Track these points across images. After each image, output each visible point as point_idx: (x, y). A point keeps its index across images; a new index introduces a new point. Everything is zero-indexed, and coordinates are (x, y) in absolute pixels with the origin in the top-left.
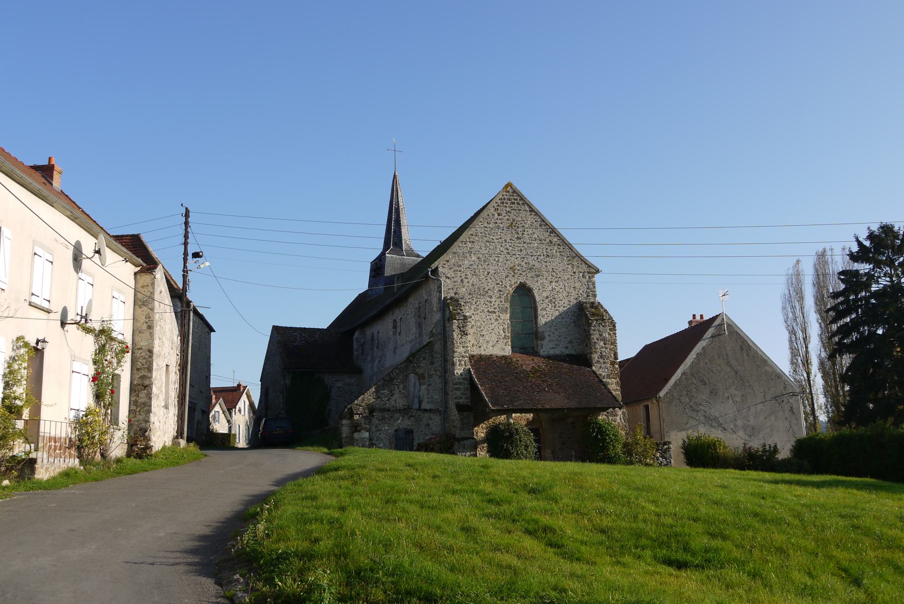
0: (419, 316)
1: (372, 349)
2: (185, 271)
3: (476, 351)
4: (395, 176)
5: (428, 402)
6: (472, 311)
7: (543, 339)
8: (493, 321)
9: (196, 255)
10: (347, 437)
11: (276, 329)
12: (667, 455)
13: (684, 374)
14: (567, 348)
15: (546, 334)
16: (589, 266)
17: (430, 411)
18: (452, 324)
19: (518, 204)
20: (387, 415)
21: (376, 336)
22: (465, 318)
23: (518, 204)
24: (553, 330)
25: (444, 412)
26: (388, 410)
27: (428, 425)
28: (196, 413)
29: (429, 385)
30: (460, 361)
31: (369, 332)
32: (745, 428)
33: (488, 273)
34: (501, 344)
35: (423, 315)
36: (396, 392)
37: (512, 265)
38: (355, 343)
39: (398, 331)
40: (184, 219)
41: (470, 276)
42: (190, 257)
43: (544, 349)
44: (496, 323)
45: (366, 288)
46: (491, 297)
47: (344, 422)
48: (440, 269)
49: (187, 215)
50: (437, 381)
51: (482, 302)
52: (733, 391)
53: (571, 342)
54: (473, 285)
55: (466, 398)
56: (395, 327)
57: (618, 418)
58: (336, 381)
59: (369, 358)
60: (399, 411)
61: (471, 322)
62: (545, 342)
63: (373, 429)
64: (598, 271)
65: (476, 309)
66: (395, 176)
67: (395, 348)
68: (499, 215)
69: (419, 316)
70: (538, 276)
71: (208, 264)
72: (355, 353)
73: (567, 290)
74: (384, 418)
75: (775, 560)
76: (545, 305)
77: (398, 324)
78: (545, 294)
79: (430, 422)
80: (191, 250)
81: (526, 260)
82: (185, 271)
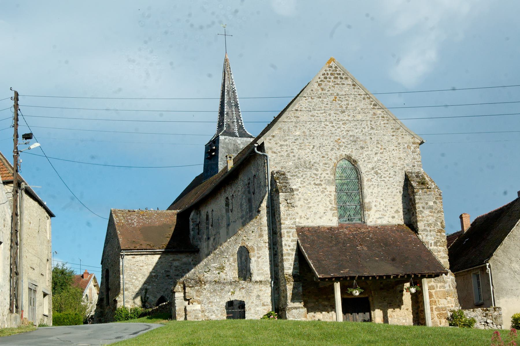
0: (249, 192)
1: (208, 228)
2: (17, 153)
3: (304, 223)
4: (226, 60)
5: (258, 275)
6: (299, 185)
7: (370, 209)
8: (320, 193)
9: (28, 137)
12: (499, 320)
15: (373, 205)
18: (278, 197)
19: (341, 78)
20: (217, 287)
22: (292, 190)
23: (341, 78)
24: (379, 200)
27: (258, 296)
28: (37, 295)
29: (258, 258)
30: (288, 232)
31: (203, 213)
34: (330, 214)
35: (252, 191)
38: (191, 223)
39: (230, 207)
40: (13, 103)
41: (296, 150)
42: (20, 138)
43: (370, 220)
44: (322, 196)
45: (202, 172)
46: (317, 170)
48: (266, 145)
49: (16, 99)
51: (309, 175)
54: (299, 159)
56: (227, 205)
57: (447, 285)
58: (174, 260)
59: (205, 237)
61: (297, 195)
65: (303, 182)
66: (226, 60)
67: (228, 225)
68: (322, 89)
69: (249, 192)
70: (362, 148)
71: (37, 145)
72: (192, 233)
73: (393, 161)
74: (215, 290)
75: (508, 261)
76: (370, 177)
77: (230, 201)
78: (370, 166)
79: (261, 294)
80: (21, 133)
82: (17, 153)
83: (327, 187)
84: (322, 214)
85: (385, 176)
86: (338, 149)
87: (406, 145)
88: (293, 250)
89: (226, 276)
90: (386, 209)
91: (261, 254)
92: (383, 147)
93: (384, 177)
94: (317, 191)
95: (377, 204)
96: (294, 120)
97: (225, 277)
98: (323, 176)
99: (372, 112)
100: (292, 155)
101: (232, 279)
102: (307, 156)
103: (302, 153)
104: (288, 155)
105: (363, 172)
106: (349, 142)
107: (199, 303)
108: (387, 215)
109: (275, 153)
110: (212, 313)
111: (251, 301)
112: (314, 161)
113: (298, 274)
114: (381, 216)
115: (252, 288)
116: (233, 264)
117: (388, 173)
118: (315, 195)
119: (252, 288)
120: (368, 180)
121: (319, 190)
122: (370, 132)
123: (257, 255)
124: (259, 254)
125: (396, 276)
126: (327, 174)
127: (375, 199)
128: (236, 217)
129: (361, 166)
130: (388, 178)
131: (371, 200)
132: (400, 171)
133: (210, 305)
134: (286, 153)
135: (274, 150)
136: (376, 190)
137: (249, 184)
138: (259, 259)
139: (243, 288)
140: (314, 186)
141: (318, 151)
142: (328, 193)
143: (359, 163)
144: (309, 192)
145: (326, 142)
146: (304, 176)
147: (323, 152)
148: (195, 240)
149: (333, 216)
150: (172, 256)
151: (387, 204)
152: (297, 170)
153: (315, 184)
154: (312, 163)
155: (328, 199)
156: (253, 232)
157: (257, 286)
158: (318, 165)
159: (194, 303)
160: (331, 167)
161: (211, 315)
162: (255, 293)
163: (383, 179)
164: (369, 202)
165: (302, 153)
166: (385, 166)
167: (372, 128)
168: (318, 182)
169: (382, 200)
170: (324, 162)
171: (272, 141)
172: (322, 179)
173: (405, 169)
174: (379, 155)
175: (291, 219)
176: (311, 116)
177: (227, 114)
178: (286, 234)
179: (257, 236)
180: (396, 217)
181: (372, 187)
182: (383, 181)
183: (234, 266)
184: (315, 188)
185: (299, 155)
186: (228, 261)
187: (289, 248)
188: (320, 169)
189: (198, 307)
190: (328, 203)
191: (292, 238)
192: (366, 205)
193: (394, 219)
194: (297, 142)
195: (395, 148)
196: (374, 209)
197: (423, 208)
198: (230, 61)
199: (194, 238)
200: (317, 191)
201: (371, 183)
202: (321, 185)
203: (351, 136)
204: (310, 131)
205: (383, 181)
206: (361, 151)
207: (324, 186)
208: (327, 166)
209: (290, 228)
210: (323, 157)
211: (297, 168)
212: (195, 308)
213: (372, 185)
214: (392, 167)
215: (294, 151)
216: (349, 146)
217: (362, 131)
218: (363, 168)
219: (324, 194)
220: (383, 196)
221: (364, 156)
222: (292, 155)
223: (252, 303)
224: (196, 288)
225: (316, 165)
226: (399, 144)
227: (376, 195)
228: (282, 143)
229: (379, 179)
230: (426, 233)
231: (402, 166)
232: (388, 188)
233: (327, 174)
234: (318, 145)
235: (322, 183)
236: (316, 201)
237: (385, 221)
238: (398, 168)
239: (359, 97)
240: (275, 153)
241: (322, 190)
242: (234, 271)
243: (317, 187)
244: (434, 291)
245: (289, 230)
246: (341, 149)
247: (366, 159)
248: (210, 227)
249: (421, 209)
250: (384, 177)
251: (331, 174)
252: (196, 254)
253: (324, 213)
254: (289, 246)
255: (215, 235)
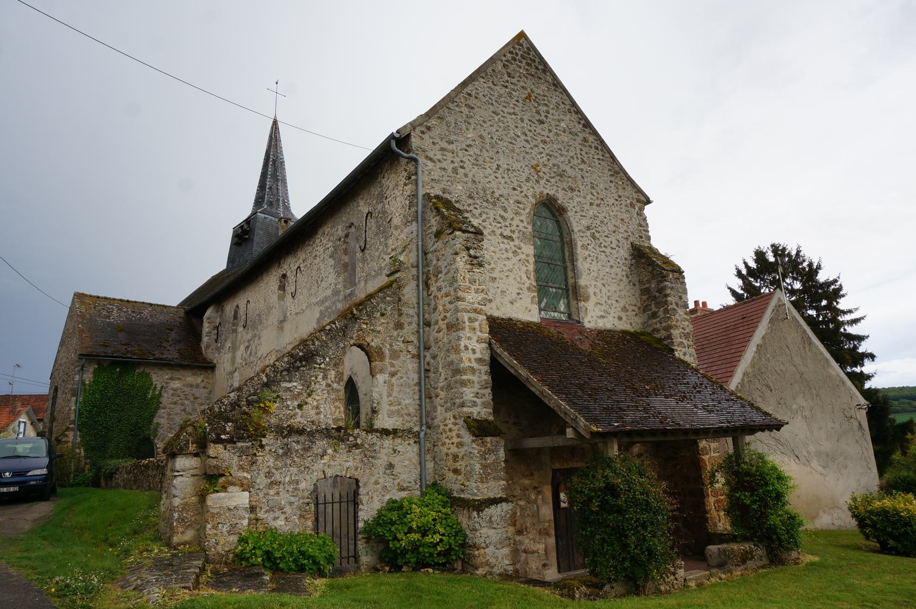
1: (235, 331)
4: (275, 123)
5: (391, 414)
7: (587, 299)
8: (510, 255)
10: (185, 507)
11: (80, 297)
13: (745, 374)
14: (620, 318)
15: (591, 291)
16: (639, 191)
17: (394, 433)
21: (242, 311)
25: (423, 433)
26: (301, 432)
27: (391, 466)
29: (393, 375)
30: (471, 320)
31: (229, 308)
32: (818, 454)
33: (498, 167)
36: (320, 386)
37: (534, 162)
41: (468, 165)
45: (224, 267)
46: (505, 210)
47: (182, 462)
50: (409, 368)
52: (801, 400)
53: (624, 309)
55: (485, 405)
58: (172, 379)
60: (326, 433)
62: (590, 305)
63: (262, 481)
64: (648, 202)
66: (275, 123)
72: (205, 339)
78: (585, 222)
79: (395, 460)
81: (553, 161)
83: (522, 245)
84: (514, 296)
85: (606, 244)
86: (537, 182)
87: (628, 202)
88: (480, 361)
89: (318, 414)
90: (609, 302)
91: (397, 368)
92: (600, 196)
93: (605, 247)
94: (507, 250)
95: (597, 291)
96: (466, 110)
97: (315, 418)
98: (515, 223)
99: (582, 135)
100: (461, 171)
101: (331, 422)
102: (487, 180)
103: (479, 174)
104: (455, 170)
105: (576, 230)
106: (553, 175)
107: (246, 486)
108: (612, 314)
109: (431, 159)
110: (278, 513)
111: (373, 480)
112: (500, 192)
113: (491, 418)
114: (602, 313)
115: (377, 448)
116: (335, 385)
117: (610, 240)
118: (503, 256)
119: (377, 448)
120: (583, 246)
121: (508, 247)
122: (581, 167)
123: (390, 369)
124: (393, 365)
125: (908, 448)
126: (522, 221)
127: (594, 283)
128: (305, 305)
129: (572, 219)
130: (609, 249)
131: (588, 283)
132: (625, 241)
133: (272, 492)
134: (451, 166)
135: (431, 154)
136: (594, 267)
137: (347, 236)
138: (394, 379)
139: (356, 446)
140: (501, 239)
141: (505, 176)
142: (524, 256)
143: (569, 214)
144: (492, 248)
145: (518, 165)
146: (484, 216)
147: (514, 180)
148: (210, 350)
149: (532, 302)
150: (169, 372)
151: (610, 294)
152: (470, 201)
153: (501, 235)
154: (496, 195)
155: (524, 269)
156: (382, 315)
157: (388, 442)
158: (506, 202)
159: (231, 488)
160: (528, 210)
161: (275, 519)
162: (383, 459)
163: (603, 249)
164: (586, 286)
165: (479, 174)
166: (605, 228)
167: (583, 162)
168: (507, 233)
169: (604, 285)
170: (516, 198)
171: (426, 136)
172: (514, 228)
173: (631, 239)
174: (595, 207)
175: (477, 291)
176: (494, 113)
177: (270, 188)
178: (467, 323)
179: (391, 325)
180: (624, 318)
181: (589, 260)
182: (603, 252)
183: (338, 391)
184: (503, 243)
185: (474, 176)
186: (325, 377)
187: (473, 357)
188: (509, 210)
189: (241, 498)
190: (524, 277)
191: (479, 333)
192: (582, 291)
193: (622, 322)
194: (471, 151)
195: (616, 202)
196: (593, 299)
197: (677, 304)
198: (280, 125)
199: (208, 347)
200: (507, 250)
201: (587, 253)
202: (510, 238)
203: (554, 165)
204: (492, 138)
205: (603, 252)
206: (570, 194)
207: (517, 242)
208: (520, 206)
209: (475, 311)
210: (514, 189)
211: (470, 197)
212: (232, 504)
213: (589, 256)
214: (614, 232)
215: (465, 165)
216: (553, 181)
217: (569, 162)
218: (577, 222)
219: (518, 258)
220: (605, 278)
221: (575, 204)
222: (461, 171)
223: (377, 483)
224: (239, 444)
225: (503, 200)
226: (620, 197)
227: (595, 274)
228: (446, 145)
229: (597, 248)
230: (683, 350)
231: (626, 234)
232: (612, 267)
233: (522, 221)
234: (505, 166)
235: (514, 236)
236: (505, 269)
237: (608, 324)
238: (621, 235)
239: (563, 106)
240: (431, 159)
241: (514, 249)
242: (337, 404)
243: (506, 241)
244: (707, 456)
245: (473, 315)
246: (542, 182)
247: (578, 209)
248: (241, 329)
249: (674, 306)
250: (605, 247)
251: (528, 223)
252: (209, 372)
253: (518, 294)
254: (474, 351)
255: (249, 341)
